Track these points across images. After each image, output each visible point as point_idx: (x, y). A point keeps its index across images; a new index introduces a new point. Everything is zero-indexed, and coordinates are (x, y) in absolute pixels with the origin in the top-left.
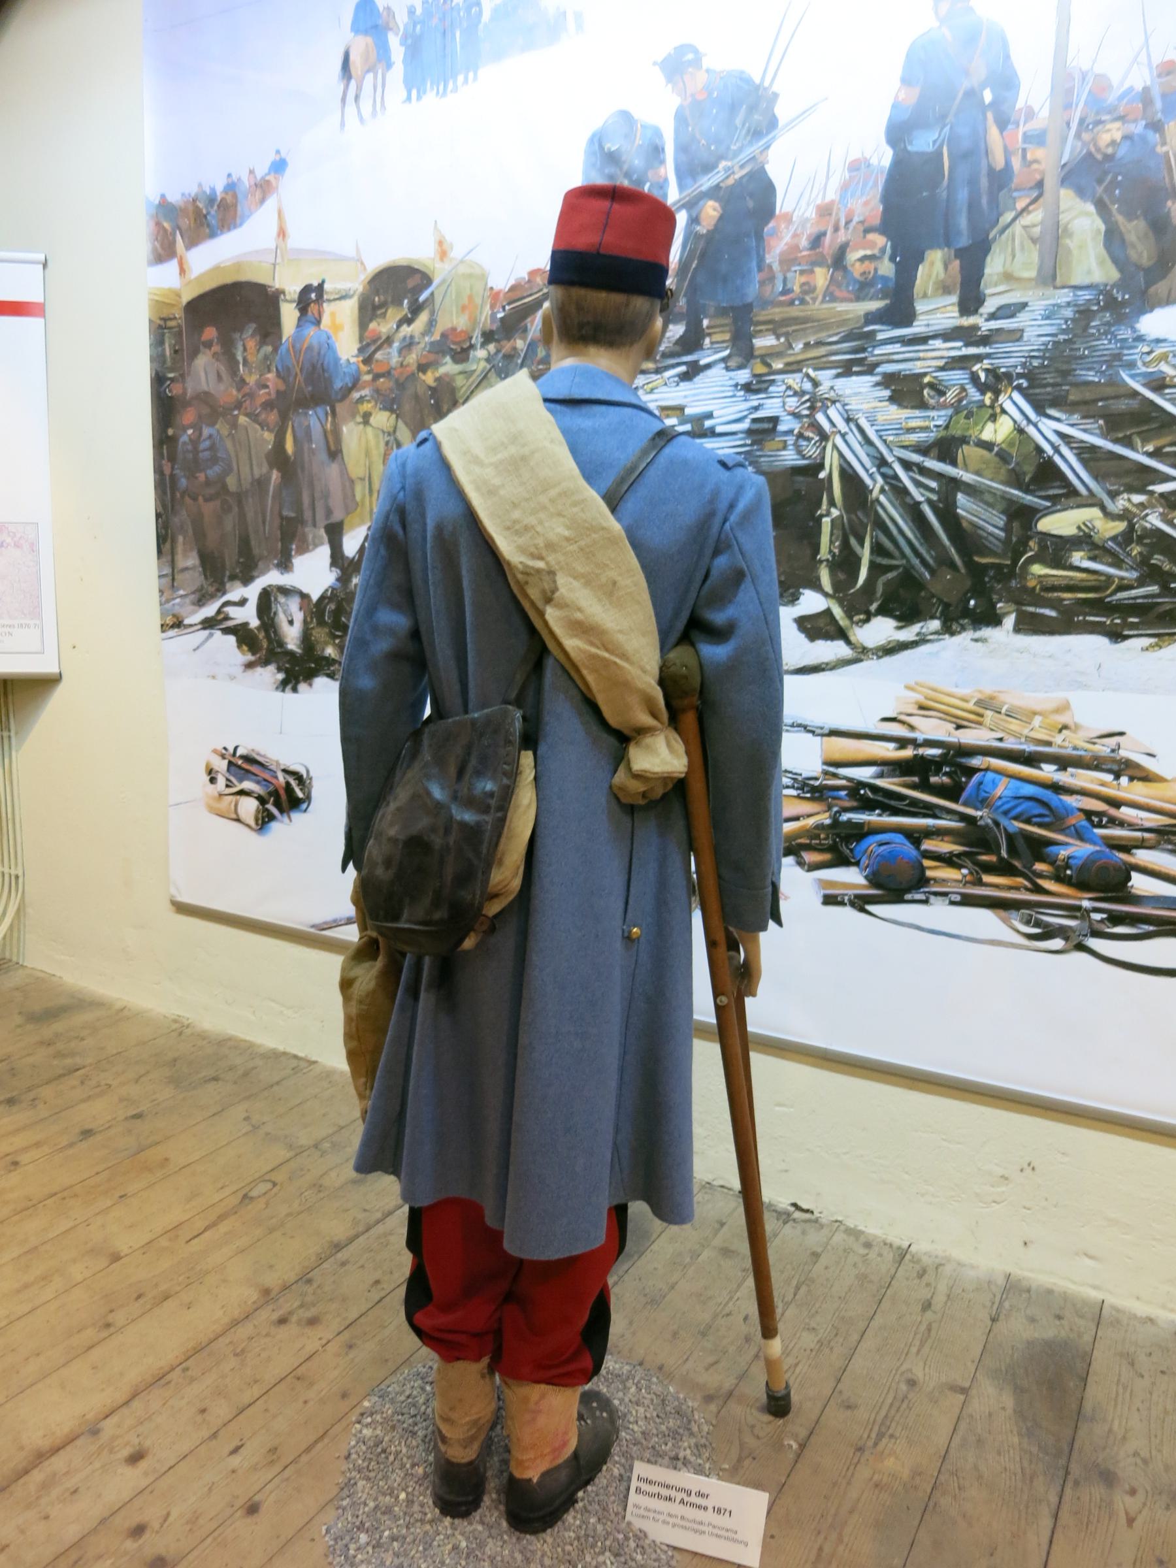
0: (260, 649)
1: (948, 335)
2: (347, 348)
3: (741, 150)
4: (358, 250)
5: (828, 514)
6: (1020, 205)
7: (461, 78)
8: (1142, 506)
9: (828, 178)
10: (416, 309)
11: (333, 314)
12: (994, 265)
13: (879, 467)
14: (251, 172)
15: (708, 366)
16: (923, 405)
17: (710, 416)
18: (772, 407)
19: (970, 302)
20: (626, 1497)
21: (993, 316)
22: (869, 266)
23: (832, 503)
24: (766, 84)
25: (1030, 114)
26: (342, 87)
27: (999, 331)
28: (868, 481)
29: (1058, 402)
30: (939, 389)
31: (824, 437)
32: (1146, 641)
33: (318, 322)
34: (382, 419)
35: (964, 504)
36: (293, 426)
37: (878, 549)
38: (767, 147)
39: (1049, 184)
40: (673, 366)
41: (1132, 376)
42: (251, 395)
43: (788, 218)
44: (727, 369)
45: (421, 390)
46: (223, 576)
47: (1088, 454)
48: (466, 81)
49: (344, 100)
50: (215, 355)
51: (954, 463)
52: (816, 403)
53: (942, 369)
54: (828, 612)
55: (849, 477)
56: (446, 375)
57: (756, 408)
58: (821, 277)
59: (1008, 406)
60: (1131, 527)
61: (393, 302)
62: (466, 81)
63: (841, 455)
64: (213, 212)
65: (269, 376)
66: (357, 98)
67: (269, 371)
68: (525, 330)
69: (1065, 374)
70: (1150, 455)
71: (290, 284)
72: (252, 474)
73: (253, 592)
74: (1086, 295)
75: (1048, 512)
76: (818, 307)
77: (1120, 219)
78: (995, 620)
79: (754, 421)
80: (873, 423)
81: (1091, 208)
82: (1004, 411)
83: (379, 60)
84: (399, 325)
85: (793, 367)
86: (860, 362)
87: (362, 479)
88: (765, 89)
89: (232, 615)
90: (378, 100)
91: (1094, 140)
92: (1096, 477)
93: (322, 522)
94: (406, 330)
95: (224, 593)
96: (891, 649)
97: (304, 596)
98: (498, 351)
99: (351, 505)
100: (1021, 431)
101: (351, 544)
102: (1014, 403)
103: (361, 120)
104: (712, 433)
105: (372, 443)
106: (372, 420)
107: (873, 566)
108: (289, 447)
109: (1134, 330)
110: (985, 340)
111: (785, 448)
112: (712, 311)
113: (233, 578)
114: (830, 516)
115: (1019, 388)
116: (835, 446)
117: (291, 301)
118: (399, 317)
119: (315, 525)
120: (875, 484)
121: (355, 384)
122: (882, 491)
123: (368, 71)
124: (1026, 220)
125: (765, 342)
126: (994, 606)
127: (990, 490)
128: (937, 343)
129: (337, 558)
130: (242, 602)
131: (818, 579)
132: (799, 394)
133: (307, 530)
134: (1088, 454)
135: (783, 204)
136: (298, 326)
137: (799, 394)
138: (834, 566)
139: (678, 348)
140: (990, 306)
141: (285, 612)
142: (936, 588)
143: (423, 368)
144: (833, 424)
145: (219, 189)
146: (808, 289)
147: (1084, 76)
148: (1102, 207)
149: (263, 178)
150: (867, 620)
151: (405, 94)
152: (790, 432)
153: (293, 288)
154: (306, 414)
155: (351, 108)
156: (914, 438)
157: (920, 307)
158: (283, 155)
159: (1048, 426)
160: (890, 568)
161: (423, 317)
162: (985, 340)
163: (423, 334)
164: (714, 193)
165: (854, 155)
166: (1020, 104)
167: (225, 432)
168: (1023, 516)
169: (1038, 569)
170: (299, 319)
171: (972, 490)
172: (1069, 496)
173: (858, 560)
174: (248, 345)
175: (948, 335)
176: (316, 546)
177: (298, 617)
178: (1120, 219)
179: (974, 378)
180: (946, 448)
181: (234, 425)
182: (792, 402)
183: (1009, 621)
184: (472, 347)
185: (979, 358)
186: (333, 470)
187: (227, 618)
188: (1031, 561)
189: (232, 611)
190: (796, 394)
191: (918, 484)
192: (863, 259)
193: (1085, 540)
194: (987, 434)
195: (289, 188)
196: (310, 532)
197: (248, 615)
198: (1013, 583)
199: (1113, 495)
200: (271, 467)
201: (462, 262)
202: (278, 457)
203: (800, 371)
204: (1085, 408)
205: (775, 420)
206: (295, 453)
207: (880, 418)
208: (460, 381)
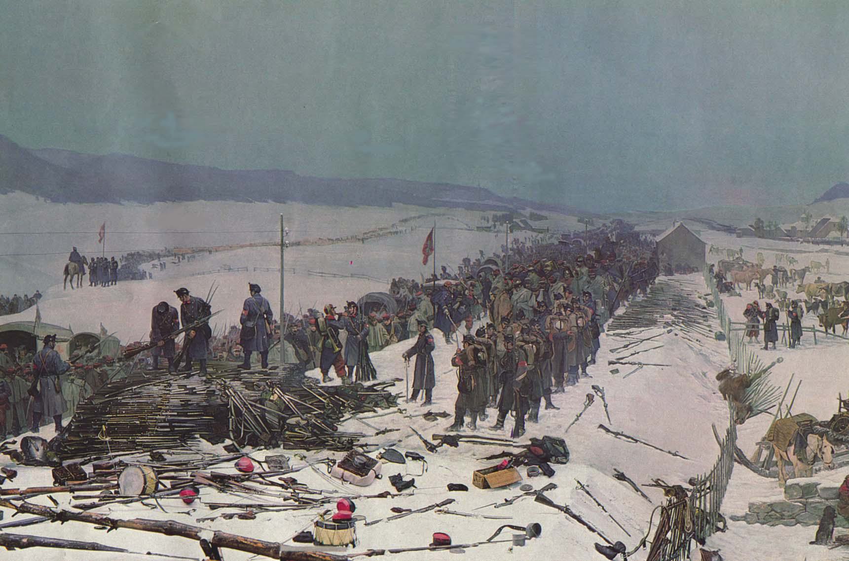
0: (22, 459)
1: (259, 373)
2: (65, 357)
3: (201, 318)
4: (70, 327)
5: (231, 418)
6: (275, 343)
7: (110, 283)
8: (310, 417)
9: (225, 329)
10: (93, 349)
11: (59, 346)
12: (270, 357)
13: (244, 405)
14: (26, 296)
15: (194, 375)
16: (254, 390)
17: (195, 388)
18: (213, 387)
19: (265, 365)
20: (699, 239)
21: (270, 369)
22: (237, 353)
23: (232, 415)
24: (744, 327)
25: (276, 322)
26: (65, 276)
27: (272, 373)
28: (242, 409)
29: (288, 392)
30: (258, 386)
31: (228, 396)
32: (315, 451)
33: (53, 348)
34: (79, 382)
35: (267, 416)
36: (40, 383)
37: (245, 427)
38: (208, 319)
39: (282, 339)
40: (183, 374)
41: (305, 386)
42: (21, 369)
43: (215, 338)
44: (199, 376)
45: (95, 374)
46: (5, 433)
47: (296, 404)
48: (112, 284)
49: (65, 280)
50: (5, 354)
51: (264, 405)
52: (225, 387)
53: (259, 381)
54: (233, 444)
55: (236, 407)
56: (105, 370)
57: (208, 388)
58: (225, 354)
59: (276, 391)
60: (308, 422)
61: (84, 345)
62: (112, 284)
63: (234, 402)
64: (7, 306)
65: (31, 363)
66: (71, 281)
67: (30, 362)
68: (133, 359)
69: (290, 384)
70: (311, 405)
71: (42, 333)
72: (21, 397)
73: (19, 439)
74: (292, 366)
75: (289, 418)
76: (224, 362)
77: (298, 349)
78: (279, 446)
79: (208, 391)
80: (241, 393)
81: (291, 346)
82: (275, 393)
83: (80, 271)
84: (87, 352)
85: (219, 377)
86: (237, 378)
87: (70, 401)
88: (747, 327)
89: (8, 447)
90: (79, 283)
91: (291, 330)
92: (299, 409)
93: (52, 414)
94: (88, 354)
95: (6, 439)
97: (44, 441)
98: (123, 365)
99: (65, 409)
100: (280, 398)
101: (65, 423)
102: (278, 391)
103: (72, 288)
104: (195, 393)
105: (75, 389)
106: (74, 382)
107: (244, 431)
108: (38, 388)
109: (304, 375)
110: (269, 375)
111: (217, 399)
112: (194, 360)
113: (9, 434)
115: (278, 387)
116: (232, 399)
117: (41, 340)
118: (86, 350)
119: (49, 415)
120: (244, 410)
121: (68, 369)
122: (245, 412)
123: (76, 274)
124: (277, 346)
125: (209, 370)
126: (278, 443)
127: (274, 413)
128: (257, 375)
129: (59, 427)
130: (14, 442)
131: (230, 435)
132: (221, 384)
133: (46, 417)
134: (296, 404)
135: (214, 334)
136: (44, 348)
137: (221, 384)
138: (233, 432)
139: (184, 369)
140: (270, 366)
141: (34, 446)
142: (262, 437)
143: (96, 367)
144: (231, 393)
145: (11, 298)
146: (222, 357)
147: (288, 315)
148: (294, 346)
149: (31, 298)
150: (244, 447)
151: (90, 284)
152: (219, 394)
153: (43, 335)
154: (47, 378)
155: (68, 284)
156: (252, 398)
157: (252, 365)
158: (40, 292)
159: (286, 397)
160: (250, 432)
161: (96, 351)
162: (269, 375)
163: (96, 356)
164: (194, 329)
165: (232, 325)
166: (273, 319)
167: (8, 381)
168: (284, 419)
169: (287, 432)
170: (45, 346)
171: (269, 412)
172: (292, 415)
173: (241, 430)
174: (20, 352)
175: (259, 373)
176: (49, 423)
177: (41, 448)
178: (298, 349)
179: (267, 383)
181: (13, 379)
182: (219, 386)
183: (282, 446)
184: (114, 362)
185: (268, 379)
186: (58, 397)
187: (6, 448)
188: (286, 430)
189: (8, 446)
190: (219, 384)
191: (254, 410)
192: (236, 351)
193: (298, 424)
194: (271, 398)
195: (41, 303)
196: (46, 418)
197: (18, 447)
198: (282, 436)
199: (303, 414)
200: (30, 395)
201: (110, 336)
202: (33, 391)
203: (220, 378)
204: (294, 393)
205: (214, 391)
206: (41, 391)
207: (243, 393)
208: (109, 372)
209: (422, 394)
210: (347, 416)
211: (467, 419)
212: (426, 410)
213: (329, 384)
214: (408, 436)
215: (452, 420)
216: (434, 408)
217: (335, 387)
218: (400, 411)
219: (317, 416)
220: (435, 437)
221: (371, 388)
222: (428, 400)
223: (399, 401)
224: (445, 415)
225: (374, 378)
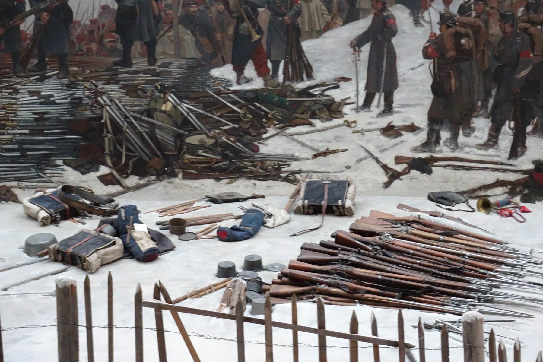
19: (152, 60)
35: (159, 133)
96: (138, 187)
102: (171, 98)
114: (108, 137)
168: (179, 138)
172: (194, 130)
180: (149, 113)
193: (202, 146)
209: (379, 99)
210: (271, 131)
211: (445, 135)
212: (384, 122)
213: (247, 87)
214: (360, 160)
215: (422, 137)
216: (397, 120)
217: (255, 92)
218: (348, 124)
219: (229, 133)
220: (399, 160)
221: (305, 92)
222: (388, 109)
223: (346, 109)
224: (412, 129)
225: (310, 77)
